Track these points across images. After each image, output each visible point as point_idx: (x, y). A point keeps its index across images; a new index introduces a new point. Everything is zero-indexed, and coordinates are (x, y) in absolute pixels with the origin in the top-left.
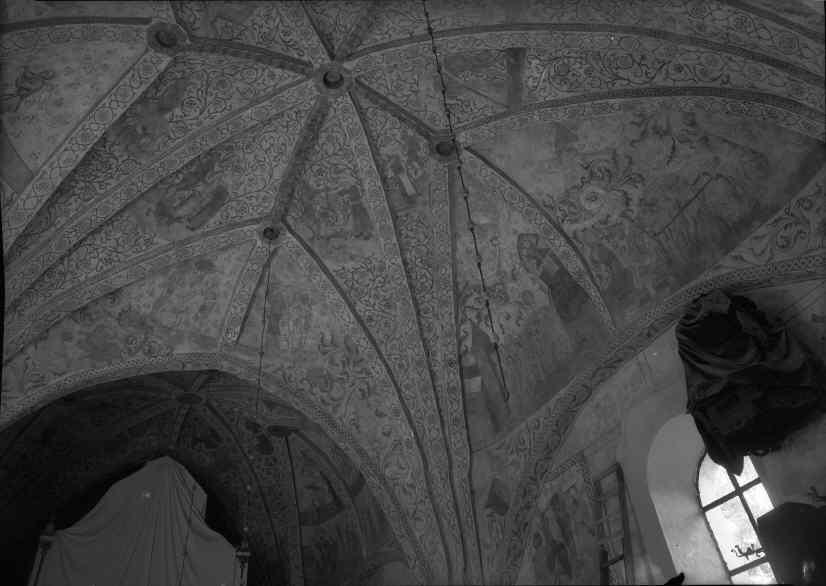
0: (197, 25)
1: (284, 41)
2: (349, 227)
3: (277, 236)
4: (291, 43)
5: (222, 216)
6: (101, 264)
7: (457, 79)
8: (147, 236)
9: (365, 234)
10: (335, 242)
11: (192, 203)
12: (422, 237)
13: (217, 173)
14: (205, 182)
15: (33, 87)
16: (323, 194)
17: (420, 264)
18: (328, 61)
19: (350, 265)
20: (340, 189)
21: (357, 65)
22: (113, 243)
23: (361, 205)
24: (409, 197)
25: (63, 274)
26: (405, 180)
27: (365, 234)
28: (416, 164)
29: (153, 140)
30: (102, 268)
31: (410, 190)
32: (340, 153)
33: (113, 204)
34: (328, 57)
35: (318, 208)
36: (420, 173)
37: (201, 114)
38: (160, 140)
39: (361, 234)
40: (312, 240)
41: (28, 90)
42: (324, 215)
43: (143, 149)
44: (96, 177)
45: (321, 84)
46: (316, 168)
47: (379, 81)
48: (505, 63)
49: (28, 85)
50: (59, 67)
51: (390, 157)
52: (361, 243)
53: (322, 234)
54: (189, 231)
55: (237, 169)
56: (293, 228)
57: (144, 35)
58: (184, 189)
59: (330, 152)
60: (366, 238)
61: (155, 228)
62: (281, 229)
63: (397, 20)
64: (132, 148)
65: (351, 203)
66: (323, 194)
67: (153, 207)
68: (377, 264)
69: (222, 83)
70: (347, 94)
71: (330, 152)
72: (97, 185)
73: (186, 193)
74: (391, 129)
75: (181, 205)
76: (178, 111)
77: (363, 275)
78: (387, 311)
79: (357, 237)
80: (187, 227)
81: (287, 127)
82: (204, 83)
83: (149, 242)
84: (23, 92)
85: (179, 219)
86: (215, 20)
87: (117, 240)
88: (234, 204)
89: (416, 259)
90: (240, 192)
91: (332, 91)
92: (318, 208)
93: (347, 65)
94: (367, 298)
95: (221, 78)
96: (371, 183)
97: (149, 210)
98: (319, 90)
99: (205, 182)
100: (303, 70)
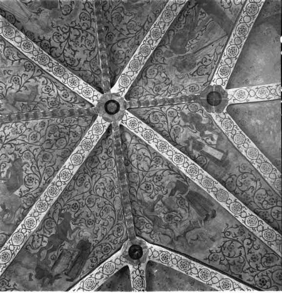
1: (67, 102)
2: (195, 217)
3: (141, 253)
4: (73, 100)
5: (92, 261)
7: (188, 53)
9: (210, 213)
10: (191, 235)
11: (64, 260)
12: (253, 184)
14: (68, 241)
17: (269, 206)
18: (100, 95)
19: (215, 247)
21: (120, 86)
23: (191, 192)
24: (221, 161)
26: (209, 150)
27: (210, 213)
28: (207, 132)
31: (218, 156)
32: (153, 163)
34: (98, 93)
35: (162, 215)
36: (215, 137)
37: (40, 183)
38: (18, 212)
40: (171, 243)
42: (170, 218)
43: (8, 222)
45: (106, 115)
46: (143, 186)
47: (144, 94)
48: (203, 11)
51: (187, 142)
52: (212, 222)
53: (177, 234)
58: (52, 250)
59: (146, 168)
60: (214, 216)
62: (141, 242)
63: (126, 45)
65: (184, 196)
68: (236, 231)
69: (45, 157)
71: (146, 168)
74: (173, 121)
75: (55, 264)
77: (231, 248)
78: (272, 264)
79: (206, 220)
80: (68, 280)
81: (106, 167)
82: (33, 160)
85: (58, 276)
88: (98, 248)
89: (262, 204)
91: (116, 115)
92: (162, 215)
93: (114, 90)
94: (247, 266)
96: (185, 165)
97: (31, 275)
98: (107, 120)
99: (68, 241)
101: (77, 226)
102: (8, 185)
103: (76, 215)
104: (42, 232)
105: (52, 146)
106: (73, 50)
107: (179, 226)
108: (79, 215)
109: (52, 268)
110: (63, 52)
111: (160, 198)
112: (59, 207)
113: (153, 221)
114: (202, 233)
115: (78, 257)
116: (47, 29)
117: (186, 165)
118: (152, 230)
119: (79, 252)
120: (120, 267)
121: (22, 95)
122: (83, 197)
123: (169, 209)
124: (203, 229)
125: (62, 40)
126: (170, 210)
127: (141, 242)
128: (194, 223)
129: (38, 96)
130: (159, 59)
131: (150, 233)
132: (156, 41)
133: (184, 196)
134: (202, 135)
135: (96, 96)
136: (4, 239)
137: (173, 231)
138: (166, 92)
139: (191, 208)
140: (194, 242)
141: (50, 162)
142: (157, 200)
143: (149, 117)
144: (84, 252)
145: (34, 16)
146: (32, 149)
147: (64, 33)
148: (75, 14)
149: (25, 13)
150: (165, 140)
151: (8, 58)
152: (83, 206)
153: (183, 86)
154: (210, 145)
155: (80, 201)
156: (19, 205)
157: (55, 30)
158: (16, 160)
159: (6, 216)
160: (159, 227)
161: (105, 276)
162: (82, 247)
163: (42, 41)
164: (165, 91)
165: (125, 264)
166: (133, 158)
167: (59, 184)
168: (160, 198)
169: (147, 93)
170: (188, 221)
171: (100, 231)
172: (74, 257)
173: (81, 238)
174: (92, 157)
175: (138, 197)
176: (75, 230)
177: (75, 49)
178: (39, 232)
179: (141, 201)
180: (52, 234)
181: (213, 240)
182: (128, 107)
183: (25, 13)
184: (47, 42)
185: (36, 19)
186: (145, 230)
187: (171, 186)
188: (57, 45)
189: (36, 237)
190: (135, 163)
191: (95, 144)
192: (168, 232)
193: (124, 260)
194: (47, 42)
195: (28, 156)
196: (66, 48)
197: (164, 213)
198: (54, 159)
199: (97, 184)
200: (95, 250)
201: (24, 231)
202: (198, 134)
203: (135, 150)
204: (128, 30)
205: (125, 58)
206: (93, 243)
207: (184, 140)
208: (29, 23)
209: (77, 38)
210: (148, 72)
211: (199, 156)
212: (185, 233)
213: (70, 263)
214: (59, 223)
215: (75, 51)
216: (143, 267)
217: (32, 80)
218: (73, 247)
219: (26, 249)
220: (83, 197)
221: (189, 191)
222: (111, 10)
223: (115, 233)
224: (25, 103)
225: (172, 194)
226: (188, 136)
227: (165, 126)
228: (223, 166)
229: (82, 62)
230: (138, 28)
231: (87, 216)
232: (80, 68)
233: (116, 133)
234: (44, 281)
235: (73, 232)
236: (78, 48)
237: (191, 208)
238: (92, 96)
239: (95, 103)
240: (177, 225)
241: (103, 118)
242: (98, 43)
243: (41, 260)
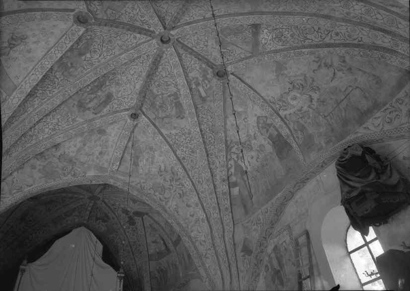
1: (141, 21)
2: (174, 112)
5: (110, 108)
6: (50, 131)
8: (73, 117)
9: (181, 116)
10: (166, 120)
11: (95, 101)
12: (209, 117)
13: (108, 86)
15: (16, 43)
17: (208, 131)
18: (163, 30)
19: (173, 132)
20: (169, 94)
23: (179, 102)
24: (203, 98)
26: (201, 89)
28: (206, 81)
29: (76, 69)
31: (203, 94)
32: (169, 76)
33: (56, 101)
34: (163, 29)
36: (208, 86)
37: (100, 56)
38: (79, 69)
40: (155, 119)
41: (14, 45)
42: (161, 107)
44: (48, 88)
45: (160, 42)
46: (157, 83)
47: (188, 40)
49: (14, 42)
50: (29, 33)
51: (193, 78)
52: (179, 121)
53: (160, 116)
54: (94, 115)
55: (118, 84)
56: (145, 113)
58: (92, 94)
59: (164, 75)
60: (182, 118)
62: (140, 113)
63: (197, 10)
64: (65, 73)
65: (174, 101)
66: (161, 96)
67: (76, 103)
69: (110, 41)
71: (164, 75)
72: (48, 92)
73: (93, 96)
74: (194, 64)
75: (90, 102)
76: (88, 55)
79: (177, 117)
80: (93, 113)
81: (142, 63)
82: (101, 41)
83: (74, 120)
84: (12, 46)
85: (89, 109)
86: (107, 10)
87: (58, 119)
88: (116, 101)
91: (165, 45)
92: (158, 103)
93: (172, 32)
95: (110, 39)
96: (184, 91)
97: (74, 104)
98: (158, 44)
99: (102, 90)
105: (117, 36)
109: (87, 104)
111: (163, 94)
115: (104, 102)
134: (203, 80)
136: (103, 222)
154: (203, 87)
159: (71, 70)
167: (112, 65)
169: (190, 41)
181: (175, 128)
192: (156, 113)
199: (132, 67)
202: (201, 79)
205: (192, 17)
223: (129, 99)
224: (114, 12)
225: (169, 96)
226: (196, 76)
228: (202, 100)
231: (118, 80)
239: (157, 33)
241: (157, 43)
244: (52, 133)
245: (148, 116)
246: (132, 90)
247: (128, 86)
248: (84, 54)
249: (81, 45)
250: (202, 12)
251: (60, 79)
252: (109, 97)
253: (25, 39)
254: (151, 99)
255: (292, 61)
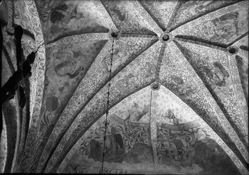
0: (152, 78)
2: (232, 21)
6: (236, 107)
8: (229, 90)
9: (235, 14)
11: (219, 74)
13: (208, 65)
14: (211, 69)
15: (172, 115)
16: (216, 31)
18: (159, 41)
20: (214, 25)
22: (229, 101)
25: (236, 118)
29: (192, 85)
30: (237, 107)
33: (211, 101)
35: (223, 33)
38: (192, 84)
39: (236, 16)
41: (173, 116)
42: (226, 30)
44: (202, 103)
45: (168, 41)
46: (205, 35)
49: (171, 116)
50: (167, 108)
53: (235, 31)
54: (229, 77)
55: (208, 58)
56: (231, 42)
57: (155, 91)
58: (212, 76)
61: (225, 87)
62: (230, 48)
63: (141, 24)
64: (194, 92)
65: (220, 21)
66: (216, 31)
67: (217, 87)
70: (170, 33)
71: (198, 31)
72: (205, 103)
73: (214, 76)
74: (183, 14)
75: (218, 78)
76: (183, 78)
79: (237, 17)
80: (228, 77)
83: (231, 90)
84: (173, 117)
86: (151, 73)
87: (228, 100)
88: (221, 61)
90: (216, 58)
93: (159, 35)
95: (172, 66)
97: (218, 88)
99: (211, 69)
100: (163, 48)
101: (206, 64)
102: (180, 83)
103: (202, 62)
104: (204, 78)
106: (136, 45)
107: (232, 29)
108: (203, 61)
109: (220, 80)
110: (136, 49)
111: (214, 30)
112: (196, 68)
113: (223, 37)
114: (242, 21)
116: (126, 54)
117: (208, 18)
118: (227, 40)
119: (218, 67)
120: (235, 58)
121: (148, 69)
122: (196, 57)
123: (222, 29)
124: (240, 20)
125: (130, 49)
126: (223, 29)
127: (230, 48)
128: (235, 22)
129: (150, 63)
130: (153, 12)
131: (228, 41)
132: (146, 13)
133: (220, 21)
135: (159, 43)
137: (232, 32)
138: (169, 13)
139: (227, 21)
140: (243, 26)
141: (177, 65)
142: (215, 32)
143: (176, 23)
144: (219, 66)
145: (120, 58)
146: (170, 70)
147: (128, 47)
148: (123, 43)
149: (118, 61)
150: (191, 22)
151: (133, 71)
152: (200, 58)
153: (171, 5)
155: (197, 59)
156: (190, 82)
157: (127, 51)
158: (172, 77)
160: (227, 36)
161: (235, 65)
162: (216, 65)
163: (130, 57)
164: (168, 13)
165: (235, 56)
166: (190, 34)
168: (214, 30)
170: (232, 24)
171: (213, 57)
172: (219, 70)
173: (213, 64)
174: (182, 50)
175: (208, 39)
176: (208, 65)
177: (135, 44)
178: (203, 79)
179: (211, 39)
180: (206, 74)
182: (169, 32)
183: (118, 61)
184: (131, 55)
185: (121, 58)
186: (225, 42)
187: (212, 24)
188: (132, 51)
189: (205, 81)
190: (193, 34)
191: (178, 49)
193: (232, 56)
194: (131, 55)
195: (172, 72)
196: (134, 48)
197: (222, 32)
198: (177, 64)
200: (220, 62)
201: (201, 86)
203: (188, 33)
204: (135, 22)
206: (217, 61)
207: (195, 12)
208: (122, 61)
209: (131, 43)
210: (156, 18)
211: (206, 9)
212: (237, 28)
213: (221, 73)
214: (202, 70)
215: (136, 44)
216: (240, 50)
217: (144, 64)
218: (214, 68)
219: (208, 86)
220: (196, 57)
221: (219, 19)
222: (126, 29)
224: (152, 69)
225: (216, 25)
227: (184, 17)
229: (141, 43)
230: (137, 18)
232: (144, 44)
233: (177, 39)
234: (223, 85)
235: (209, 66)
236: (135, 43)
237: (227, 21)
238: (158, 45)
239: (162, 44)
240: (231, 29)
242: (188, 116)
243: (214, 82)
244: (238, 106)
245: (234, 40)
246: (211, 50)
247: (208, 53)
248: (182, 80)
249: (174, 83)
250: (140, 21)
251: (197, 95)
252: (217, 65)
253: (170, 110)
254: (218, 38)
255: (84, 57)
